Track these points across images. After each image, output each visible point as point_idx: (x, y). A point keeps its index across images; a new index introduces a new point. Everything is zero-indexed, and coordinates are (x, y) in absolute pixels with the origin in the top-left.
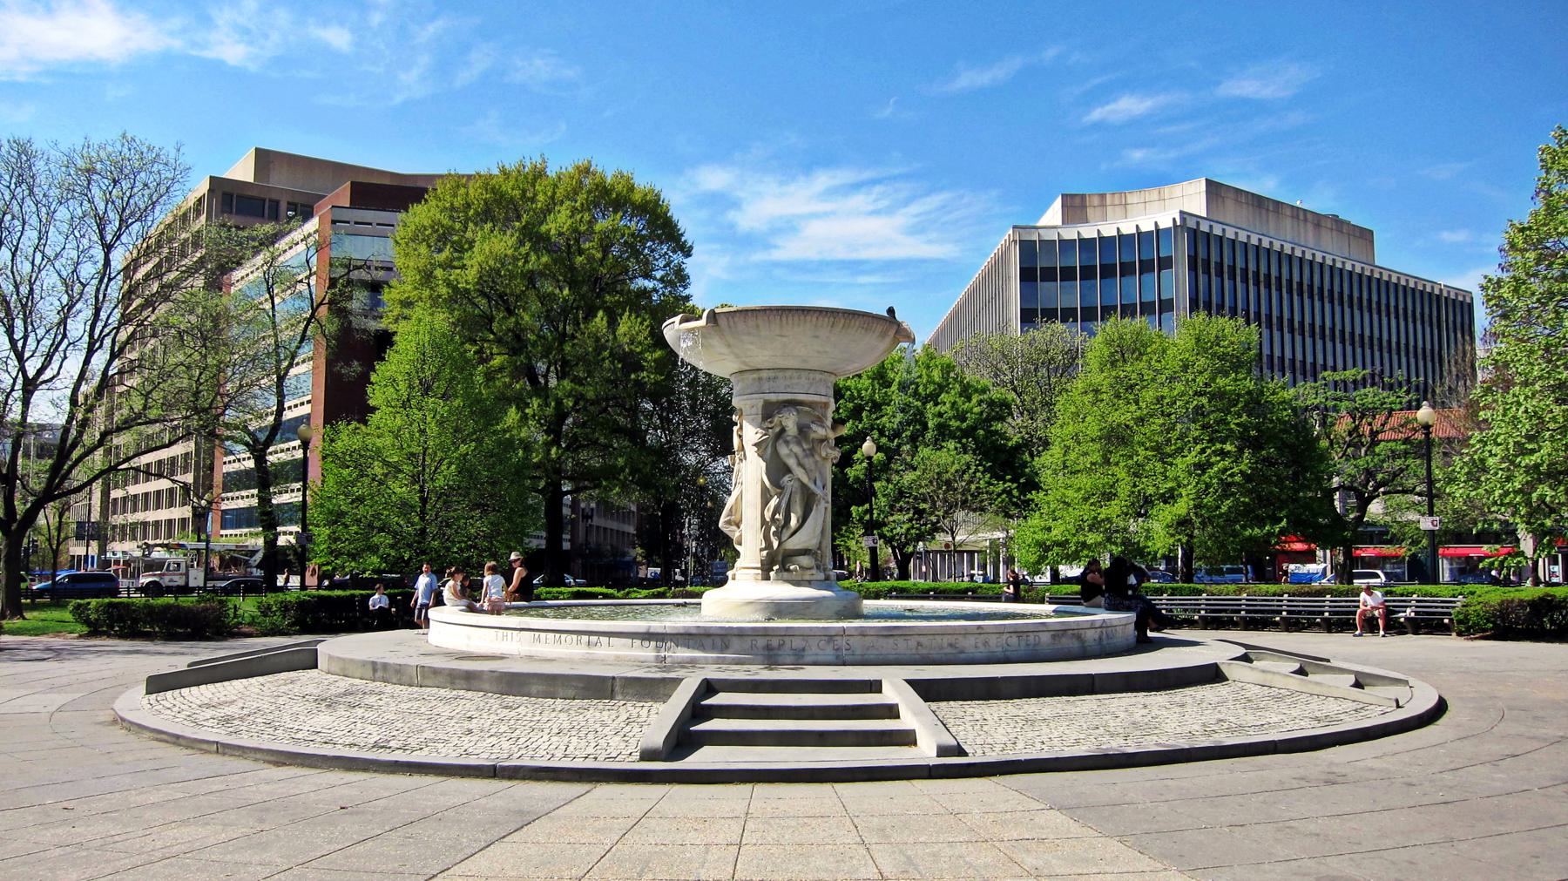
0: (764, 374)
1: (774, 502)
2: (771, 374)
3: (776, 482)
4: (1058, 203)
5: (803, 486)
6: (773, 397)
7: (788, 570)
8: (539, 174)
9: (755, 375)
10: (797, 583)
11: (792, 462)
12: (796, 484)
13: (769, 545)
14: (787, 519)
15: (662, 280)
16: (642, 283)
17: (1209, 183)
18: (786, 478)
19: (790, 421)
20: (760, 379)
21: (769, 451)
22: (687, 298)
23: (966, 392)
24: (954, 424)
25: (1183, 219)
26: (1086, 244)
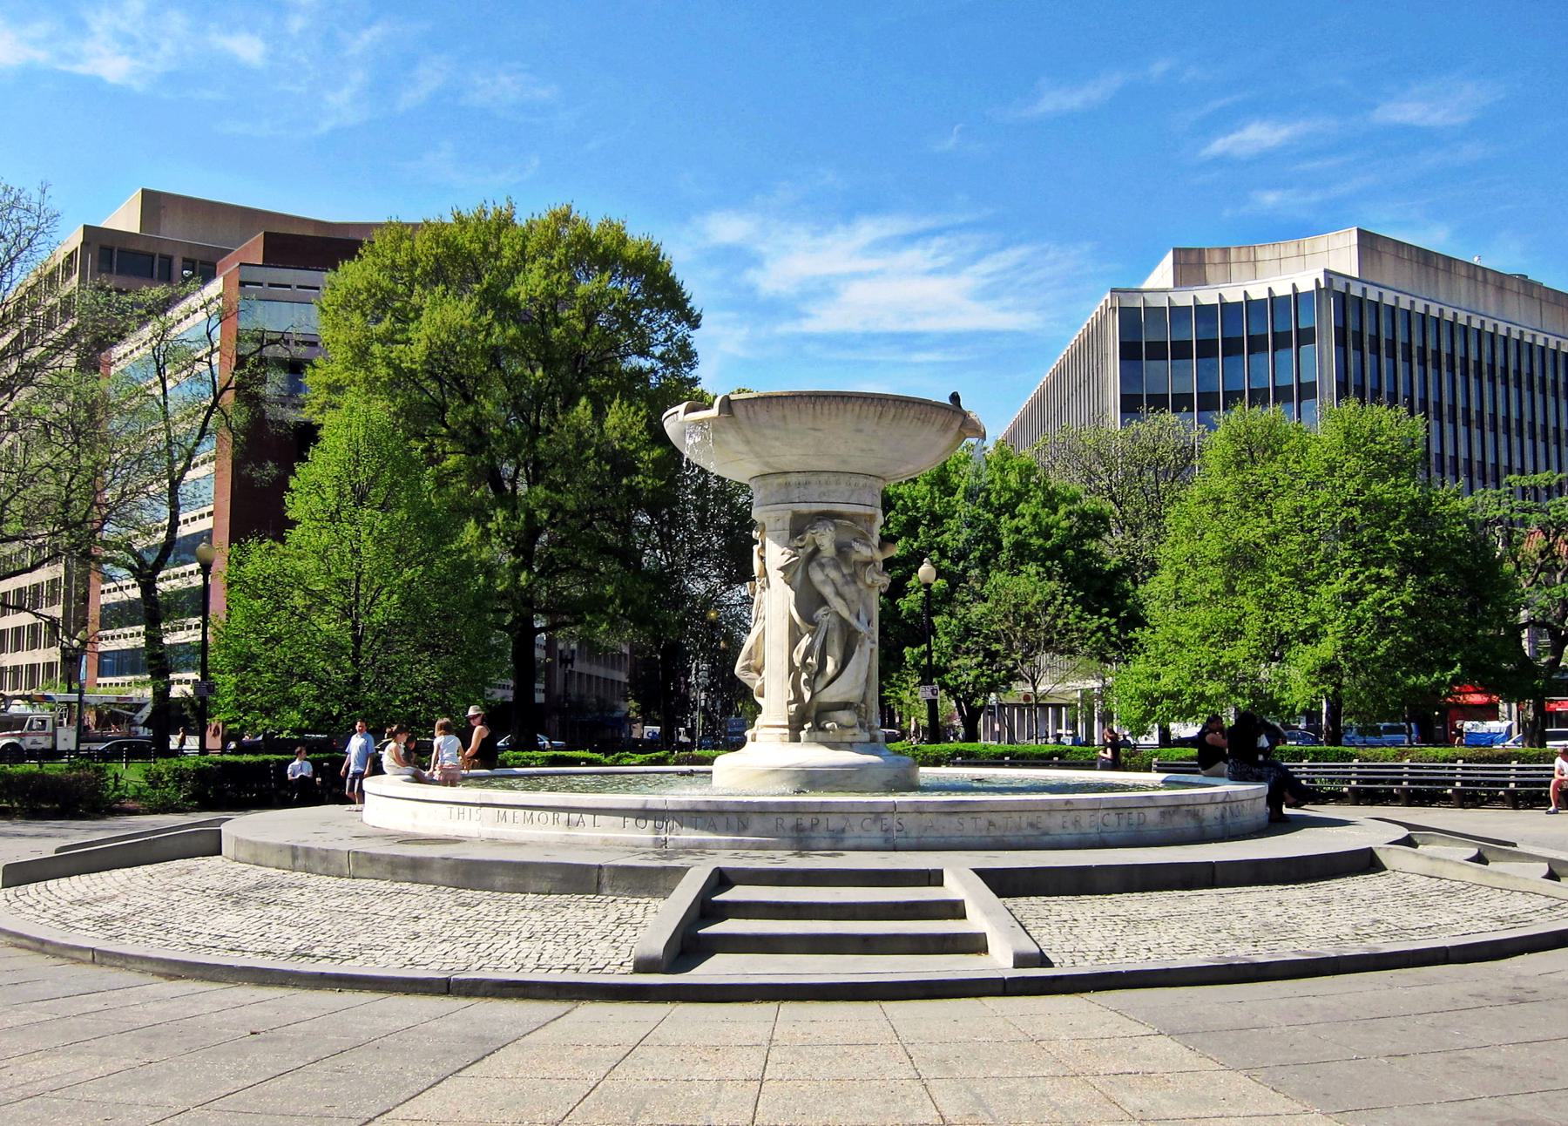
0: (793, 479)
1: (805, 642)
3: (808, 617)
5: (843, 622)
6: (804, 508)
9: (781, 480)
10: (835, 746)
11: (828, 591)
12: (834, 619)
13: (799, 697)
14: (822, 664)
15: (662, 358)
16: (636, 362)
18: (821, 612)
19: (826, 539)
20: (787, 485)
21: (799, 576)
22: (695, 381)
23: (1051, 500)
24: (1036, 542)
25: (1329, 281)
26: (1205, 312)
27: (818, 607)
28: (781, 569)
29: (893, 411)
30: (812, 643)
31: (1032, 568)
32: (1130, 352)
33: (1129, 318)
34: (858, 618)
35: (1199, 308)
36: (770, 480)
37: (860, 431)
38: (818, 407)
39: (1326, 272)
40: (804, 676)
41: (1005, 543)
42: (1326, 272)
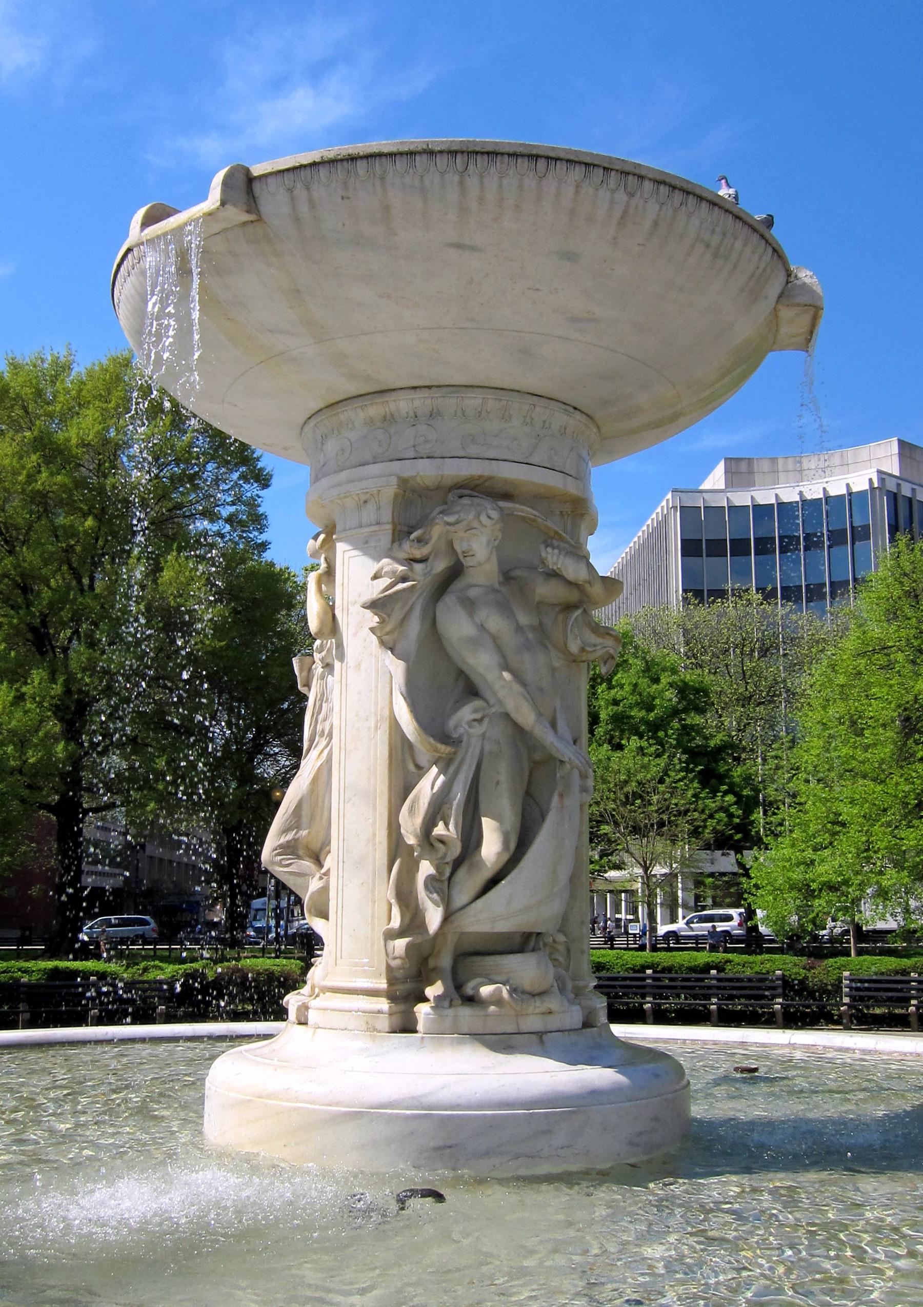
0: (402, 404)
1: (428, 785)
2: (421, 402)
3: (434, 724)
4: (720, 469)
5: (519, 732)
6: (426, 472)
7: (472, 1000)
8: (61, 368)
9: (375, 410)
10: (503, 1042)
11: (481, 662)
12: (498, 731)
13: (413, 922)
14: (471, 838)
15: (229, 520)
16: (203, 524)
17: (901, 443)
18: (467, 713)
19: (478, 539)
20: (389, 420)
21: (415, 627)
22: (264, 546)
23: (652, 672)
24: (638, 714)
25: (882, 481)
26: (762, 511)
27: (459, 703)
28: (374, 605)
29: (653, 208)
30: (447, 789)
31: (634, 742)
32: (690, 548)
33: (688, 513)
34: (553, 725)
35: (757, 507)
36: (345, 414)
37: (570, 257)
38: (472, 183)
39: (879, 472)
40: (426, 868)
41: (603, 715)
42: (879, 472)
